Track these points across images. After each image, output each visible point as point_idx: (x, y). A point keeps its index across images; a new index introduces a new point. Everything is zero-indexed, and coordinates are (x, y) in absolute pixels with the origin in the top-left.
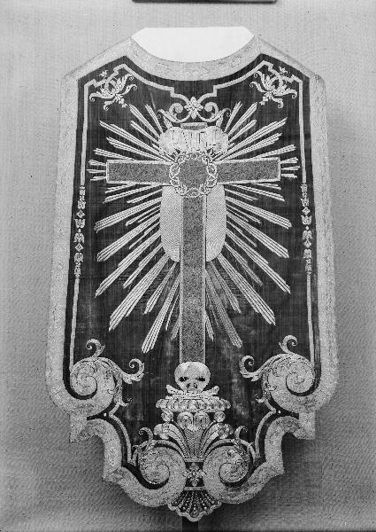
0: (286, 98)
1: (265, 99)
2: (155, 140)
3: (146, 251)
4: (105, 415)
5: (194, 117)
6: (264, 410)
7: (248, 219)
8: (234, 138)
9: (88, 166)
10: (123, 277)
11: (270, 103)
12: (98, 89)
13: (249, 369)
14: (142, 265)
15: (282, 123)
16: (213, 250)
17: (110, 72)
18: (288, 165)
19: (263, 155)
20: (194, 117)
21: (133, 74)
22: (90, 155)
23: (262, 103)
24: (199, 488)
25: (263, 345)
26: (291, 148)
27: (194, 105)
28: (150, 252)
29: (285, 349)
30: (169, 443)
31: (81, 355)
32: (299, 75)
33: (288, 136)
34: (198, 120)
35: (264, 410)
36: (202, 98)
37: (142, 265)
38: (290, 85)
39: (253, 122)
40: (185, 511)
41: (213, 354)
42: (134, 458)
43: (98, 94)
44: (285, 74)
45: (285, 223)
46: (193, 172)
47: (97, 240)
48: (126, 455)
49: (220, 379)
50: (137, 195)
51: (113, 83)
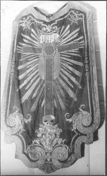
0: (79, 21)
1: (72, 23)
2: (38, 40)
3: (33, 76)
4: (17, 134)
5: (50, 31)
6: (74, 134)
7: (68, 64)
8: (63, 37)
9: (17, 47)
10: (26, 86)
11: (74, 23)
12: (21, 23)
13: (68, 118)
14: (32, 81)
15: (78, 29)
16: (55, 76)
17: (26, 18)
18: (81, 44)
19: (73, 41)
20: (50, 31)
21: (33, 19)
22: (18, 44)
23: (71, 24)
24: (50, 162)
25: (73, 109)
26: (82, 37)
27: (49, 28)
28: (34, 77)
29: (81, 110)
30: (40, 145)
31: (11, 111)
32: (83, 13)
33: (81, 33)
34: (51, 32)
35: (74, 133)
36: (52, 25)
37: (32, 81)
38: (79, 17)
39: (69, 31)
40: (45, 170)
41: (57, 112)
42: (27, 151)
43: (21, 25)
44: (78, 13)
45: (80, 64)
46: (49, 49)
47: (18, 73)
48: (24, 149)
49: (58, 122)
50: (31, 58)
51: (27, 22)
